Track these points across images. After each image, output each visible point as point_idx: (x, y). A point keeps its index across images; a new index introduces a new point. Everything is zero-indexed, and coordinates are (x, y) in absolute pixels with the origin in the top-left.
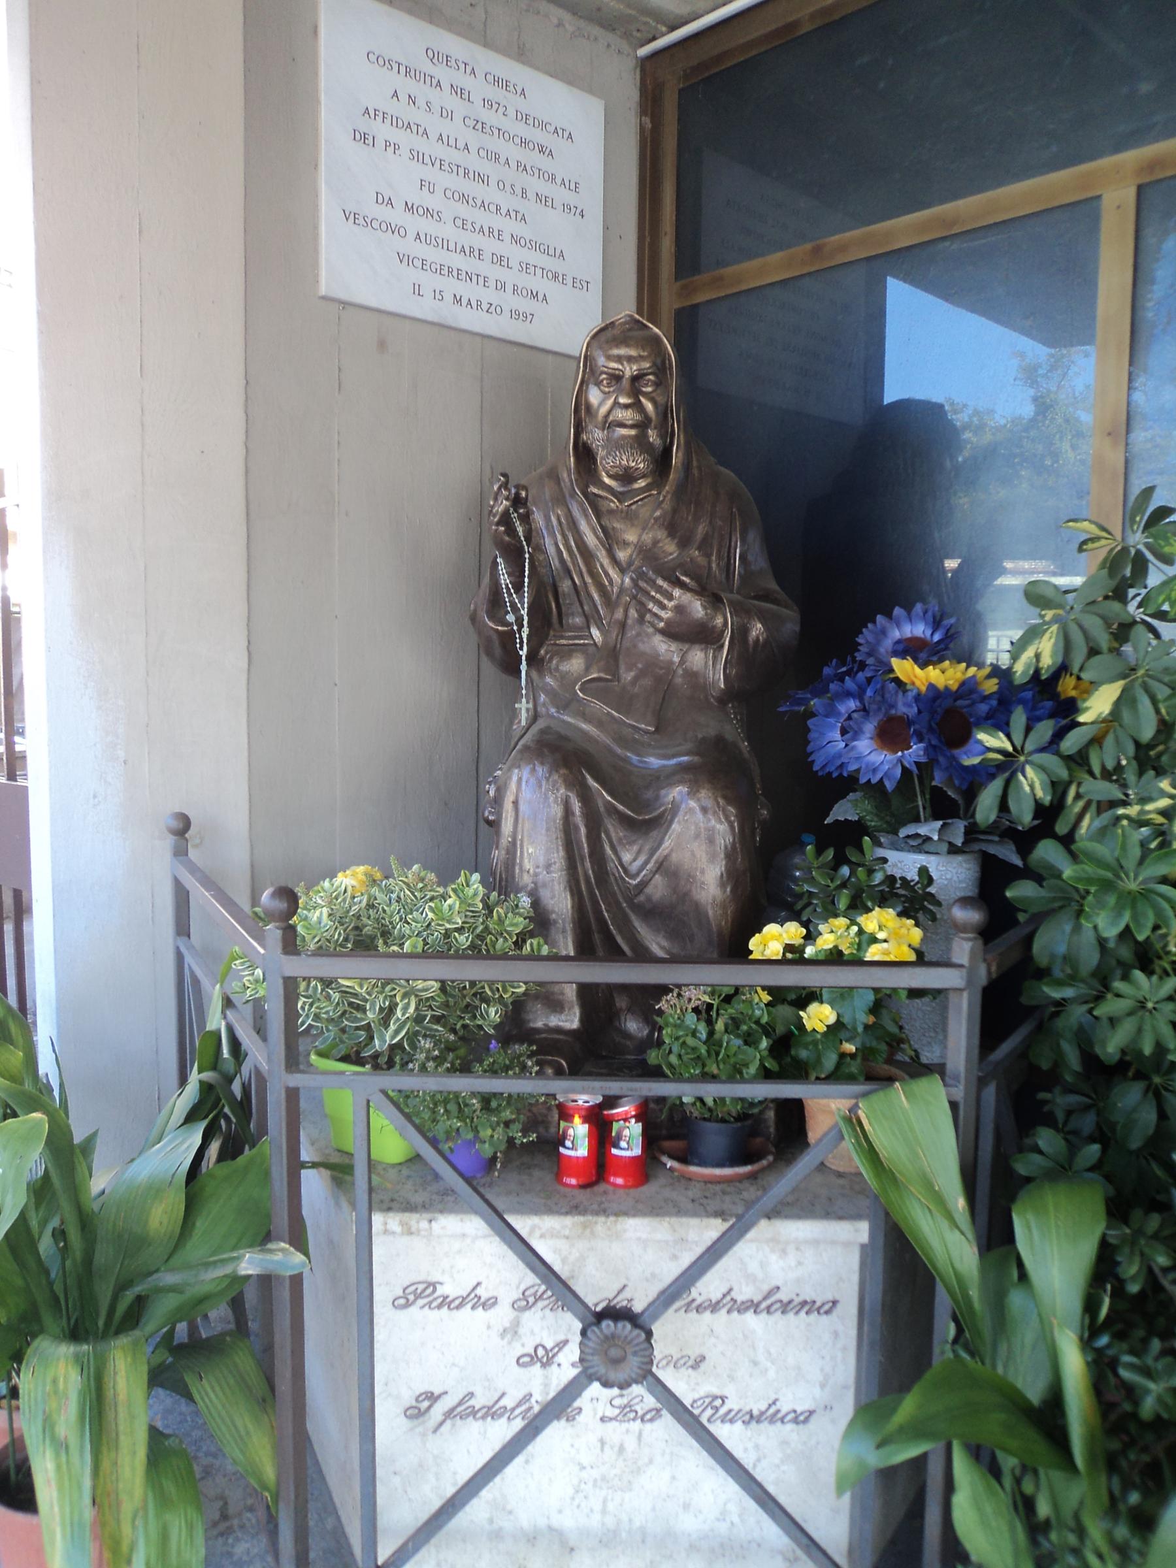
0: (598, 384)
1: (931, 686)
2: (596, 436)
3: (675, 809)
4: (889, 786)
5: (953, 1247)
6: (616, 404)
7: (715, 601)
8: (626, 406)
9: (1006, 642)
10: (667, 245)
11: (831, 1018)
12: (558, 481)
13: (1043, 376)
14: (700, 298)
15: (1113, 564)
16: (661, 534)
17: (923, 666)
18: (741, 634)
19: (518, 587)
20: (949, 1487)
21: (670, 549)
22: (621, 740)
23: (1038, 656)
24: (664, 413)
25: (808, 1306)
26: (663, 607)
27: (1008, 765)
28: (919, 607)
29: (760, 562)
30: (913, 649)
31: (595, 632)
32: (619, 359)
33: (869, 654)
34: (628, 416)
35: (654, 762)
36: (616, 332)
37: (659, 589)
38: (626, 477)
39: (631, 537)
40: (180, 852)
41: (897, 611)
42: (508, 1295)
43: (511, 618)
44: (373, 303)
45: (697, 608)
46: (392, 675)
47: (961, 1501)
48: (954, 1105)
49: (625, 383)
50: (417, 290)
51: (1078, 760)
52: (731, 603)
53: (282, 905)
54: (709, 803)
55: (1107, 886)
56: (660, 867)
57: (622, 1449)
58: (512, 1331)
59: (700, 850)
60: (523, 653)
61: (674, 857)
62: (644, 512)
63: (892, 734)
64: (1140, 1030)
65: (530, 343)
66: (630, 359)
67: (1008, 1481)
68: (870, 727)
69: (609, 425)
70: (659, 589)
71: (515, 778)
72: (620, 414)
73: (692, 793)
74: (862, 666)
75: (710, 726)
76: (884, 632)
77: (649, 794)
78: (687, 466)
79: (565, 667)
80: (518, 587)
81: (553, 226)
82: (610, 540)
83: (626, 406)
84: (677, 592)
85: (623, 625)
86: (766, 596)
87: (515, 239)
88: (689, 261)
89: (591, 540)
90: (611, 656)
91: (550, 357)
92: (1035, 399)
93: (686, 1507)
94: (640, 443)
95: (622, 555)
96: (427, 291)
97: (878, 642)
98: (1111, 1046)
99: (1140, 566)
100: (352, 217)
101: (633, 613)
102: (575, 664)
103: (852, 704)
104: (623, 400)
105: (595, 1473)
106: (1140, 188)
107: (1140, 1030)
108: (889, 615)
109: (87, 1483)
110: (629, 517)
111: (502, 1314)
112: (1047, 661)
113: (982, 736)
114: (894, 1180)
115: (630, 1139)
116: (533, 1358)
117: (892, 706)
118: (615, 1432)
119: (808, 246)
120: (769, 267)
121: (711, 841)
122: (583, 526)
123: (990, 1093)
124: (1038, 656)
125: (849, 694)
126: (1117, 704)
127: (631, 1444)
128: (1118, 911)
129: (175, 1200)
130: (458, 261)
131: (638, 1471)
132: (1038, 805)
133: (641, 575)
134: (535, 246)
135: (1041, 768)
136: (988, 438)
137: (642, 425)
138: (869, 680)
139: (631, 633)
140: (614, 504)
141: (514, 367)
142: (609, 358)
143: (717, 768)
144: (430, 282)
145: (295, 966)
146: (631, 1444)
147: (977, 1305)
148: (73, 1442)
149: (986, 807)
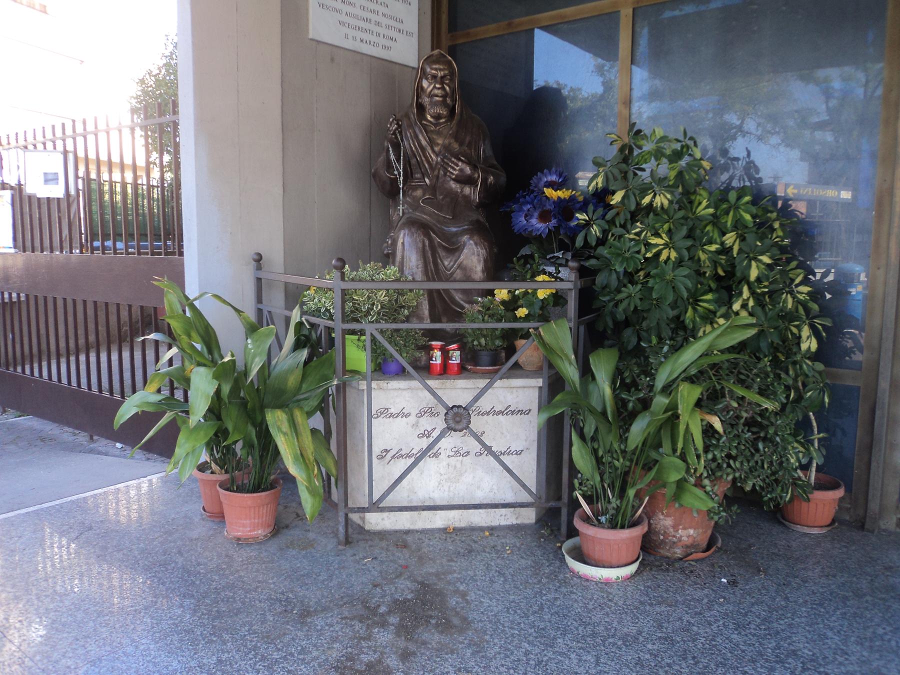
0: (427, 79)
1: (559, 198)
2: (426, 100)
3: (464, 245)
4: (544, 236)
5: (571, 372)
6: (435, 87)
7: (474, 167)
8: (439, 89)
9: (587, 180)
10: (444, 17)
11: (527, 312)
12: (409, 118)
13: (608, 71)
14: (458, 42)
15: (622, 150)
16: (452, 141)
17: (556, 191)
18: (485, 180)
19: (398, 160)
20: (571, 445)
21: (456, 146)
22: (439, 222)
23: (597, 184)
24: (453, 91)
25: (520, 412)
26: (455, 169)
27: (588, 224)
28: (554, 169)
29: (490, 153)
30: (550, 185)
31: (427, 180)
32: (436, 69)
33: (536, 187)
34: (439, 92)
35: (454, 230)
36: (434, 58)
37: (453, 162)
38: (437, 117)
39: (440, 141)
40: (259, 268)
41: (545, 171)
42: (414, 412)
43: (396, 172)
44: (330, 42)
45: (468, 170)
46: (336, 200)
47: (574, 448)
48: (571, 329)
49: (438, 79)
50: (346, 37)
51: (612, 222)
52: (481, 168)
53: (339, 264)
54: (478, 241)
55: (619, 255)
56: (459, 266)
57: (455, 467)
58: (415, 425)
59: (475, 259)
60: (401, 186)
61: (465, 262)
62: (445, 132)
63: (544, 217)
64: (629, 304)
65: (389, 59)
66: (440, 70)
67: (589, 444)
68: (536, 214)
69: (431, 96)
70: (453, 162)
71: (402, 235)
72: (436, 91)
73: (470, 238)
74: (533, 191)
75: (474, 216)
76: (541, 179)
77: (454, 240)
78: (462, 112)
79: (415, 194)
80: (398, 160)
81: (399, 9)
82: (432, 143)
83: (439, 89)
84: (460, 164)
85: (438, 177)
86: (493, 166)
87: (384, 15)
88: (453, 26)
89: (424, 143)
90: (433, 189)
91: (397, 66)
92: (603, 83)
93: (478, 488)
94: (444, 103)
95: (436, 149)
96: (350, 37)
97: (539, 183)
98: (621, 317)
99: (631, 150)
100: (322, 6)
101: (442, 172)
102: (419, 193)
103: (529, 206)
104: (437, 86)
105: (445, 477)
106: (634, 9)
107: (629, 304)
108: (542, 173)
109: (296, 443)
110: (439, 133)
111: (412, 419)
112: (600, 185)
113: (577, 215)
114: (551, 349)
115: (456, 357)
116: (424, 435)
117: (545, 206)
118: (453, 461)
119: (507, 22)
120: (490, 30)
121: (479, 255)
122: (421, 137)
123: (582, 329)
124: (597, 184)
125: (528, 203)
126: (623, 198)
127: (459, 465)
128: (622, 263)
129: (298, 373)
130: (362, 24)
131: (461, 475)
132: (598, 238)
133: (445, 157)
134: (392, 18)
135: (598, 225)
136: (579, 104)
137: (444, 96)
138: (535, 197)
139: (440, 180)
140: (433, 128)
141: (384, 71)
142: (432, 69)
143: (477, 229)
144: (351, 33)
145: (344, 286)
146: (459, 465)
147: (579, 390)
148: (289, 432)
149: (579, 241)
